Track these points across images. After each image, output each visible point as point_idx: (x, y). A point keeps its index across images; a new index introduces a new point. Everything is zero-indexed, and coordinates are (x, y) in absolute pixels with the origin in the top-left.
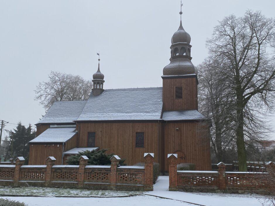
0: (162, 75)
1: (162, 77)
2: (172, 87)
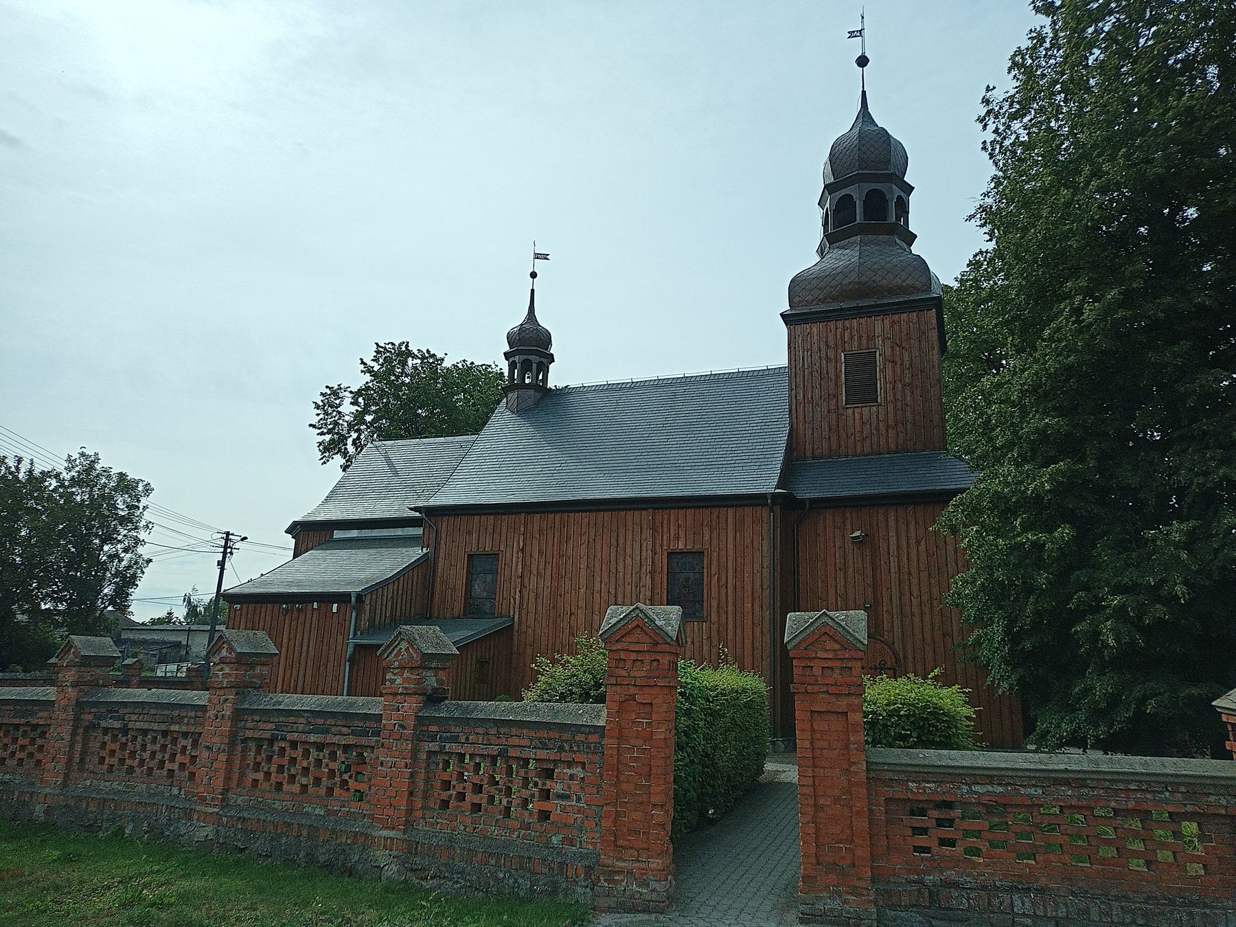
0: (785, 307)
1: (782, 315)
2: (831, 354)
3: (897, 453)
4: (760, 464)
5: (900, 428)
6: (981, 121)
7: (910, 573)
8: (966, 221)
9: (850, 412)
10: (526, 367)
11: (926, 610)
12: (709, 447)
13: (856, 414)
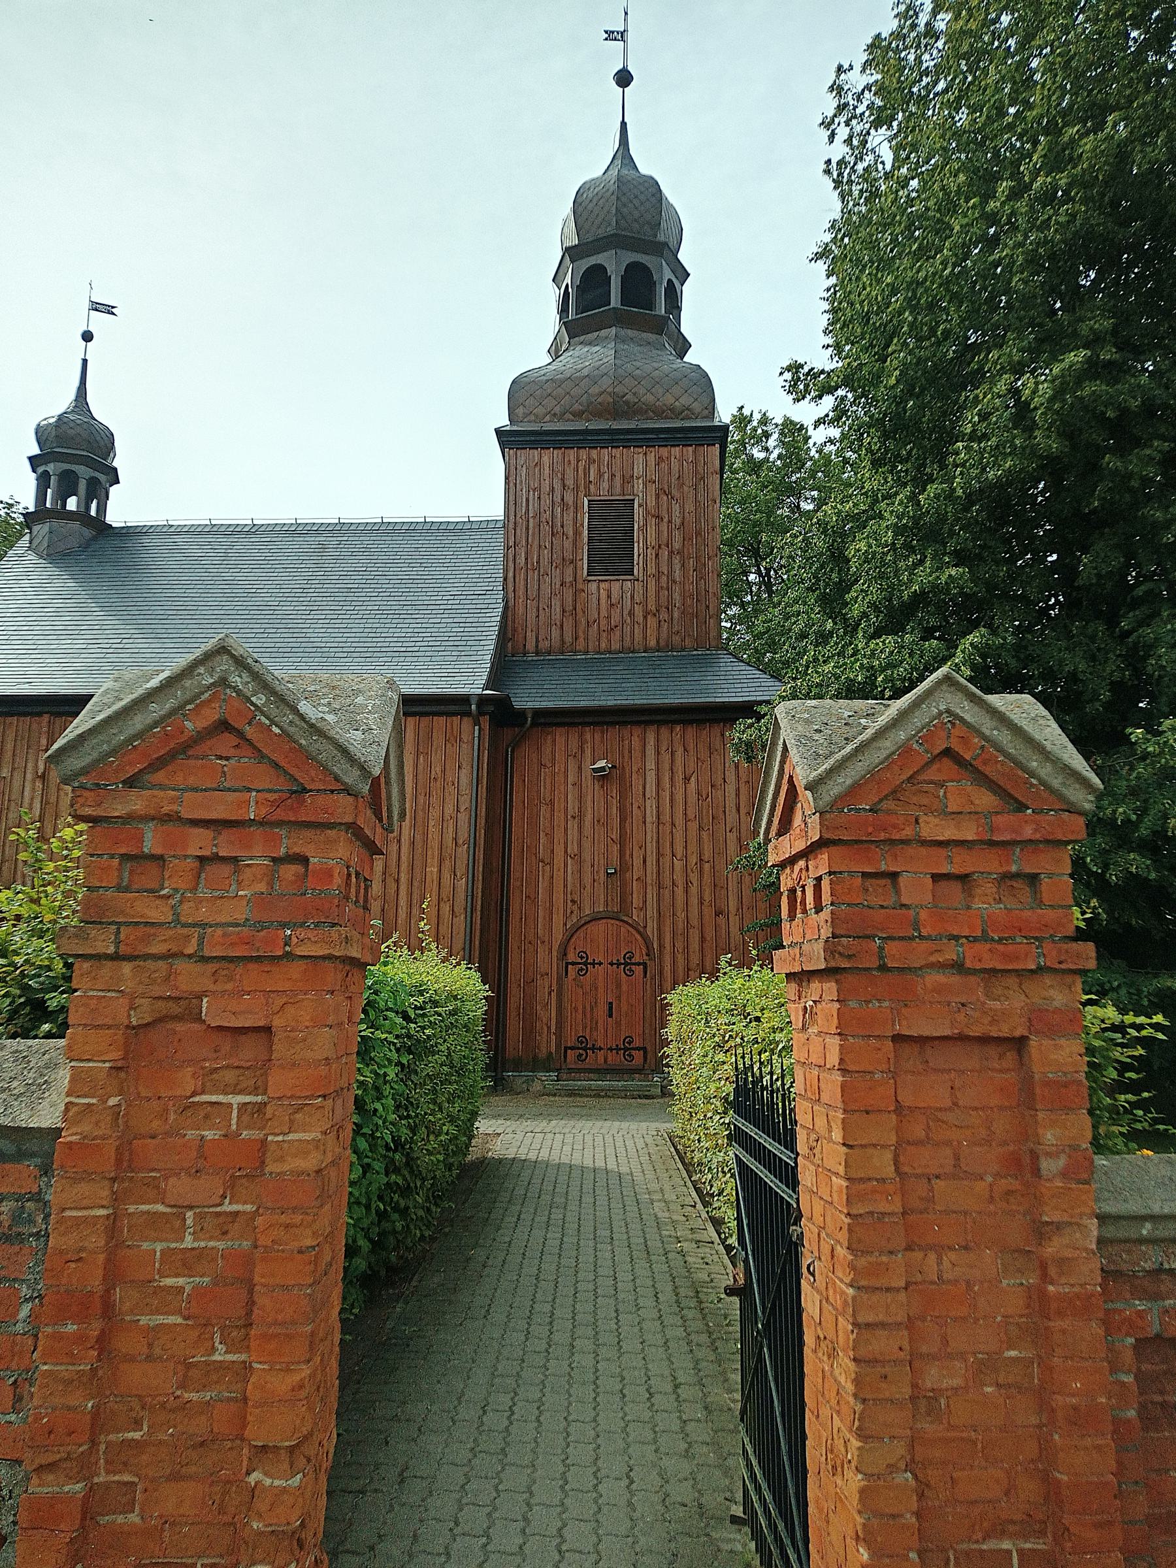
0: (503, 421)
2: (569, 498)
3: (658, 651)
4: (458, 653)
5: (664, 615)
6: (828, 127)
7: (673, 824)
8: (811, 261)
9: (593, 586)
10: (68, 486)
11: (694, 878)
12: (378, 625)
13: (602, 591)
